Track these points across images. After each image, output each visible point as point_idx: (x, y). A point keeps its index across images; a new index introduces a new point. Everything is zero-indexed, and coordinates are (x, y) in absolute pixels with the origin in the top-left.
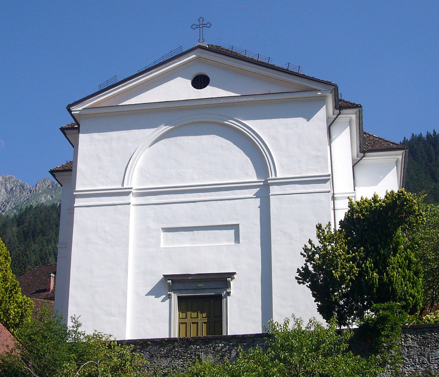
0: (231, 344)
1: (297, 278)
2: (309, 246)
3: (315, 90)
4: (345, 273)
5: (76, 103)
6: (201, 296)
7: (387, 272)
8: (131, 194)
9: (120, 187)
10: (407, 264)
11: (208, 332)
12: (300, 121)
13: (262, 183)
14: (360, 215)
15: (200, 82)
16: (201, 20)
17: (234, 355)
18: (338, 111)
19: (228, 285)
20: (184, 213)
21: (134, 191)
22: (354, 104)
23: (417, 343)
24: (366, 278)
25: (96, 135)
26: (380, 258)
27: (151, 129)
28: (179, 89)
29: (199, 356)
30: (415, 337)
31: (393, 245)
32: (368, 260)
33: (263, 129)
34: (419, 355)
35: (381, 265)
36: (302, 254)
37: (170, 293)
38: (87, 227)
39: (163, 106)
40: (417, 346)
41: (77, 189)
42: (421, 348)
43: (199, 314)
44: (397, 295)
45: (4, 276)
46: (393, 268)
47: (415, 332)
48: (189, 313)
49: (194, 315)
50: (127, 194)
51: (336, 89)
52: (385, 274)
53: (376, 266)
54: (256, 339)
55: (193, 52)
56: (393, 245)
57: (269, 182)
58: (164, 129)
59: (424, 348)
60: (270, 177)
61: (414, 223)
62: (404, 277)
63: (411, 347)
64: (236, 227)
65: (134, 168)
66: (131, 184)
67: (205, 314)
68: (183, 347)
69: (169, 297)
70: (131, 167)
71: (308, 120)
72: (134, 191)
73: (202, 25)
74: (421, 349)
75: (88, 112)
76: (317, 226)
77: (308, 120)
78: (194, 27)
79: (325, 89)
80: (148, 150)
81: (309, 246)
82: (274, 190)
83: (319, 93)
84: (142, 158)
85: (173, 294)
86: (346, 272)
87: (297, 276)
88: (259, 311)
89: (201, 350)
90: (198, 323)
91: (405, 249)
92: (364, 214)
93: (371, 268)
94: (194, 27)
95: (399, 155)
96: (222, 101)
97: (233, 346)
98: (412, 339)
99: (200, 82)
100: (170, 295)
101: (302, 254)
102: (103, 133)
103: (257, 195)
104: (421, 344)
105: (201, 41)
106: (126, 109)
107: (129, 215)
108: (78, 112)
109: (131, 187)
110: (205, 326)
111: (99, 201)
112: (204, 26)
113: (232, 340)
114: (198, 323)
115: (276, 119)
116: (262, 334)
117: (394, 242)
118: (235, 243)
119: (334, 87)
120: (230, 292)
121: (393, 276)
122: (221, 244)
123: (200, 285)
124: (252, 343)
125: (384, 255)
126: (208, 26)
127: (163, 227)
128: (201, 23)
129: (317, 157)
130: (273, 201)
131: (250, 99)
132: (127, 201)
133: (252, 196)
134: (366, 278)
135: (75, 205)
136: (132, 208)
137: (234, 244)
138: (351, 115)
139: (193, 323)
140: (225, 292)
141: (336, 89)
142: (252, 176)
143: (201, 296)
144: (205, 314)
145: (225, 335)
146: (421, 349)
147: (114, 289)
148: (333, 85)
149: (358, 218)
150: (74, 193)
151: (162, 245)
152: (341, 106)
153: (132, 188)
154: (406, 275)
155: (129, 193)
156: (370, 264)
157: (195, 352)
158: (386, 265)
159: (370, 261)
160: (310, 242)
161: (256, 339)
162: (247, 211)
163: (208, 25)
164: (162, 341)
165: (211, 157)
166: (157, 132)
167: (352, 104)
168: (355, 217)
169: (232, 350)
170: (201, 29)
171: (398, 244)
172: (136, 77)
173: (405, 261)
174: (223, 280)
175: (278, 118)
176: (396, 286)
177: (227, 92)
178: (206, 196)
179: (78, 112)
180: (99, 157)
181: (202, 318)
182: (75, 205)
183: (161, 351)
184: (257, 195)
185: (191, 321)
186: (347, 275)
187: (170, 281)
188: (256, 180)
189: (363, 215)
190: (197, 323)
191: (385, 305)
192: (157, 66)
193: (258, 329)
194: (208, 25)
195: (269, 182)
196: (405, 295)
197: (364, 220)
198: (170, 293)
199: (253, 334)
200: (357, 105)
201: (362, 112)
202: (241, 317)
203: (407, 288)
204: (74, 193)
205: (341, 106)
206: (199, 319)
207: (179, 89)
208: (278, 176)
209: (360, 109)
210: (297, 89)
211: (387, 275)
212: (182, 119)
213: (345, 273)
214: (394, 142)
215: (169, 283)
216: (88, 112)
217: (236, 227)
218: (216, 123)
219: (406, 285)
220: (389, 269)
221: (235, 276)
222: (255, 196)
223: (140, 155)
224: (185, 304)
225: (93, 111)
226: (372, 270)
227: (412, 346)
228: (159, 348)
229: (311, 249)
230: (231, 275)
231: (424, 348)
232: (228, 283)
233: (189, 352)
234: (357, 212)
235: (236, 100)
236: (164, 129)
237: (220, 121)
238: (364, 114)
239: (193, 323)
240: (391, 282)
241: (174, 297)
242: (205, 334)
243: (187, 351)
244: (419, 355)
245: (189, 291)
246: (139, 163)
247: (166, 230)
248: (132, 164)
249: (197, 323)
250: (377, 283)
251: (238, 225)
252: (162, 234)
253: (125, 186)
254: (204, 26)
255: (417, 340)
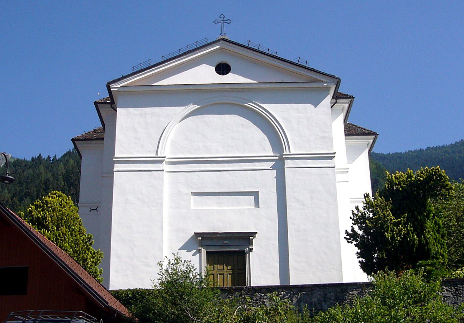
0: (292, 292)
1: (345, 238)
2: (356, 212)
3: (322, 81)
4: (396, 235)
5: (114, 81)
6: (228, 251)
7: (424, 235)
8: (164, 162)
9: (155, 155)
10: (437, 229)
11: (233, 283)
12: (309, 107)
13: (277, 158)
14: (399, 187)
15: (223, 69)
16: (222, 16)
17: (295, 302)
18: (335, 100)
19: (250, 243)
20: (210, 181)
21: (166, 160)
22: (347, 95)
23: (451, 293)
24: (408, 239)
25: (132, 110)
26: (418, 224)
27: (181, 107)
28: (204, 74)
29: (264, 302)
30: (449, 288)
31: (426, 213)
32: (409, 224)
33: (278, 111)
34: (453, 304)
35: (420, 229)
36: (351, 218)
37: (200, 248)
38: (128, 191)
39: (191, 88)
40: (452, 296)
41: (116, 156)
42: (454, 298)
43: (225, 267)
44: (431, 254)
45: (80, 230)
46: (429, 232)
47: (449, 284)
48: (216, 266)
49: (221, 267)
50: (161, 162)
51: (339, 82)
52: (423, 236)
53: (415, 230)
54: (313, 288)
55: (217, 43)
56: (426, 213)
57: (284, 156)
58: (192, 107)
59: (458, 298)
60: (285, 153)
61: (447, 195)
62: (435, 239)
63: (446, 297)
64: (256, 194)
65: (167, 140)
66: (164, 153)
67: (230, 266)
68: (249, 294)
69: (200, 251)
70: (164, 139)
71: (315, 107)
72: (166, 160)
73: (222, 21)
74: (455, 299)
75: (125, 89)
76: (364, 195)
77: (315, 107)
78: (216, 22)
79: (330, 82)
80: (178, 125)
81: (356, 212)
82: (288, 164)
83: (325, 85)
84: (173, 132)
85: (202, 249)
86: (396, 234)
87: (346, 236)
88: (277, 265)
89: (265, 297)
90: (224, 274)
91: (434, 216)
92: (402, 186)
93: (411, 231)
94: (216, 22)
95: (370, 139)
96: (243, 86)
97: (294, 294)
98: (447, 290)
99: (223, 69)
100: (201, 250)
101: (351, 218)
102: (138, 109)
103: (273, 168)
104: (454, 294)
105: (223, 34)
106: (159, 89)
107: (163, 180)
108: (117, 89)
109: (164, 156)
110: (230, 276)
111: (136, 167)
112: (219, 22)
113: (293, 290)
114: (224, 274)
115: (289, 104)
116: (280, 286)
117: (427, 211)
118: (255, 206)
119: (338, 80)
120: (252, 249)
121: (429, 238)
122: (221, 208)
123: (226, 242)
124: (310, 292)
125: (421, 220)
126: (216, 21)
127: (192, 192)
128: (222, 19)
129: (324, 137)
130: (288, 173)
131: (267, 86)
132: (161, 168)
133: (269, 168)
134: (408, 239)
135: (114, 170)
136: (166, 175)
137: (254, 207)
138: (344, 104)
139: (220, 274)
140: (247, 248)
141: (339, 82)
142: (269, 152)
143: (228, 251)
144: (230, 266)
145: (249, 285)
146: (455, 299)
147: (143, 243)
148: (337, 78)
149: (398, 189)
150: (114, 159)
151: (192, 207)
152: (337, 97)
153: (165, 157)
154: (437, 238)
155: (163, 161)
156: (410, 228)
157: (260, 299)
158: (423, 228)
159: (411, 225)
160: (357, 208)
161: (313, 288)
162: (265, 181)
163: (229, 22)
164: (230, 289)
165: (232, 133)
166: (186, 110)
167: (345, 95)
168: (395, 189)
169: (293, 297)
170: (222, 24)
171: (430, 211)
172: (168, 62)
173: (436, 226)
174: (247, 238)
175: (290, 103)
176: (430, 246)
177: (246, 79)
178: (229, 166)
179: (117, 89)
180: (133, 129)
181: (227, 270)
182: (114, 170)
183: (229, 298)
184: (273, 168)
185: (218, 273)
186: (397, 236)
187: (201, 238)
188: (272, 154)
189: (401, 187)
190: (223, 274)
191: (429, 261)
192: (186, 54)
193: (275, 281)
194: (229, 22)
195: (284, 156)
196: (436, 254)
197: (402, 192)
198: (200, 248)
199: (311, 285)
200: (350, 96)
201: (353, 102)
202: (262, 271)
203: (438, 248)
204: (114, 159)
205: (337, 97)
206: (225, 271)
207: (204, 74)
208: (292, 153)
209: (352, 99)
210: (308, 81)
211: (424, 237)
212: (208, 101)
213: (396, 235)
214: (366, 128)
215: (200, 240)
216: (125, 89)
217: (256, 194)
218: (236, 105)
219: (437, 246)
220: (426, 232)
221: (257, 235)
222: (272, 168)
223: (172, 129)
224: (213, 258)
225: (130, 89)
226: (412, 233)
227: (447, 296)
228: (227, 295)
229: (358, 214)
230: (254, 234)
231: (458, 298)
232: (251, 240)
233: (255, 299)
234: (396, 184)
235: (255, 86)
236: (192, 107)
237: (241, 104)
238: (354, 104)
239: (220, 274)
240: (427, 243)
241: (204, 252)
242: (230, 286)
243: (253, 298)
244: (453, 304)
245: (233, 246)
246: (171, 135)
247: (195, 194)
248: (165, 137)
249: (223, 274)
250: (417, 244)
251: (258, 192)
252: (192, 198)
253: (159, 155)
254: (219, 22)
255: (451, 291)
